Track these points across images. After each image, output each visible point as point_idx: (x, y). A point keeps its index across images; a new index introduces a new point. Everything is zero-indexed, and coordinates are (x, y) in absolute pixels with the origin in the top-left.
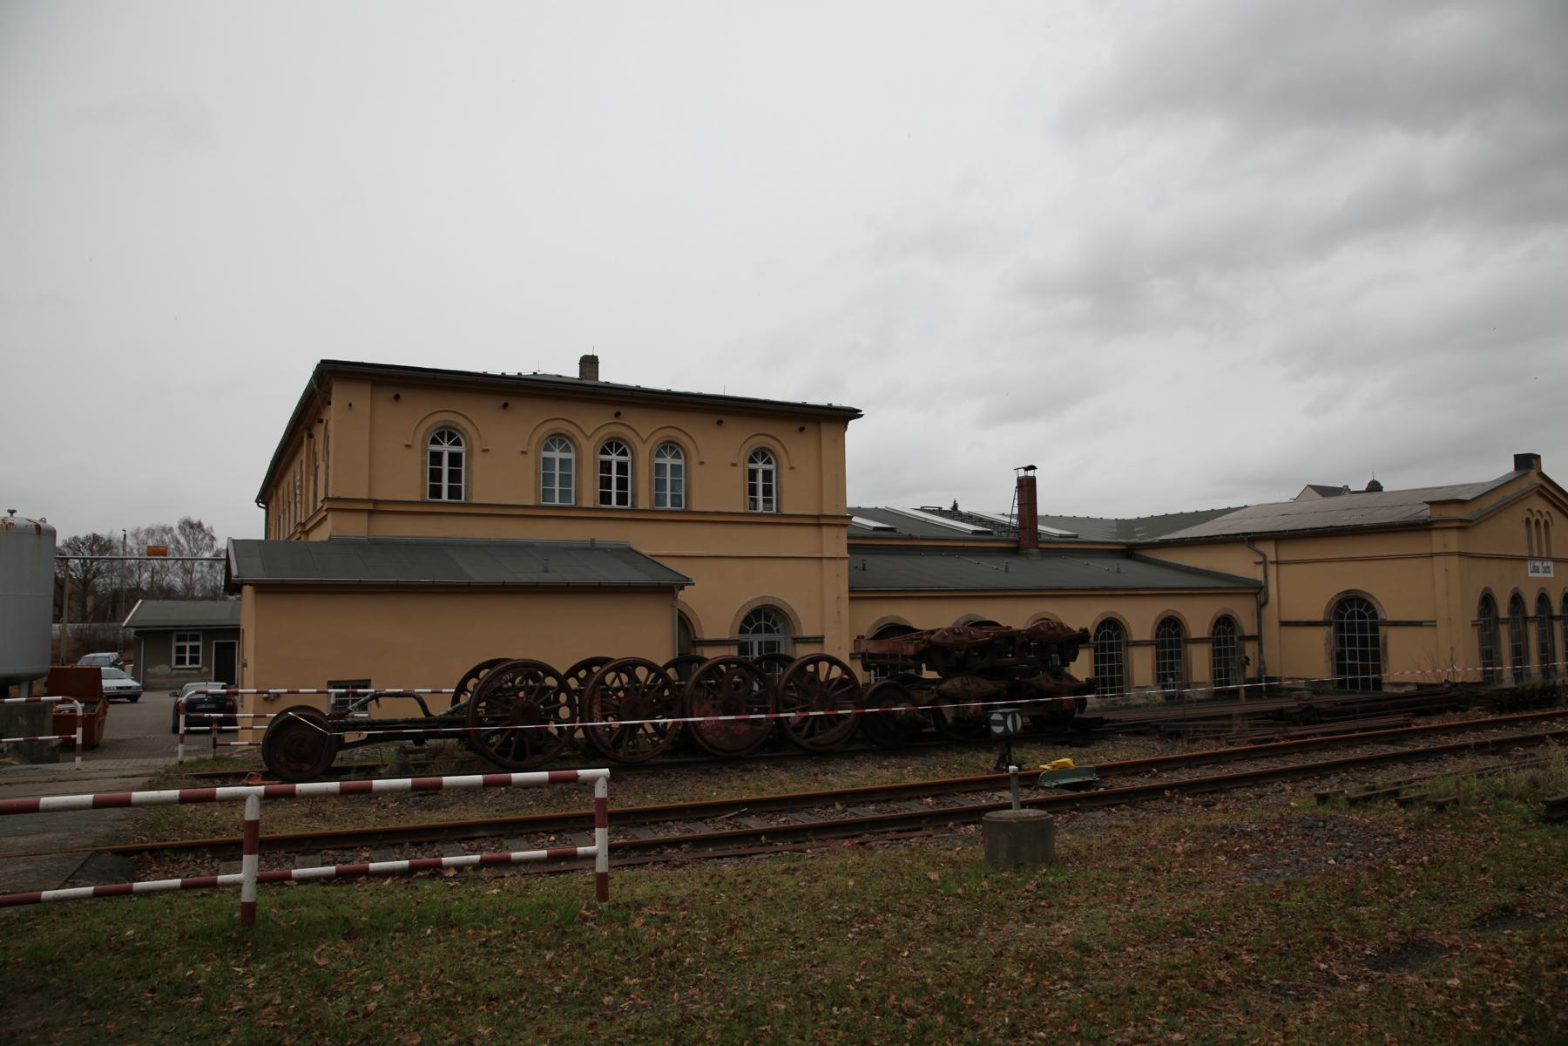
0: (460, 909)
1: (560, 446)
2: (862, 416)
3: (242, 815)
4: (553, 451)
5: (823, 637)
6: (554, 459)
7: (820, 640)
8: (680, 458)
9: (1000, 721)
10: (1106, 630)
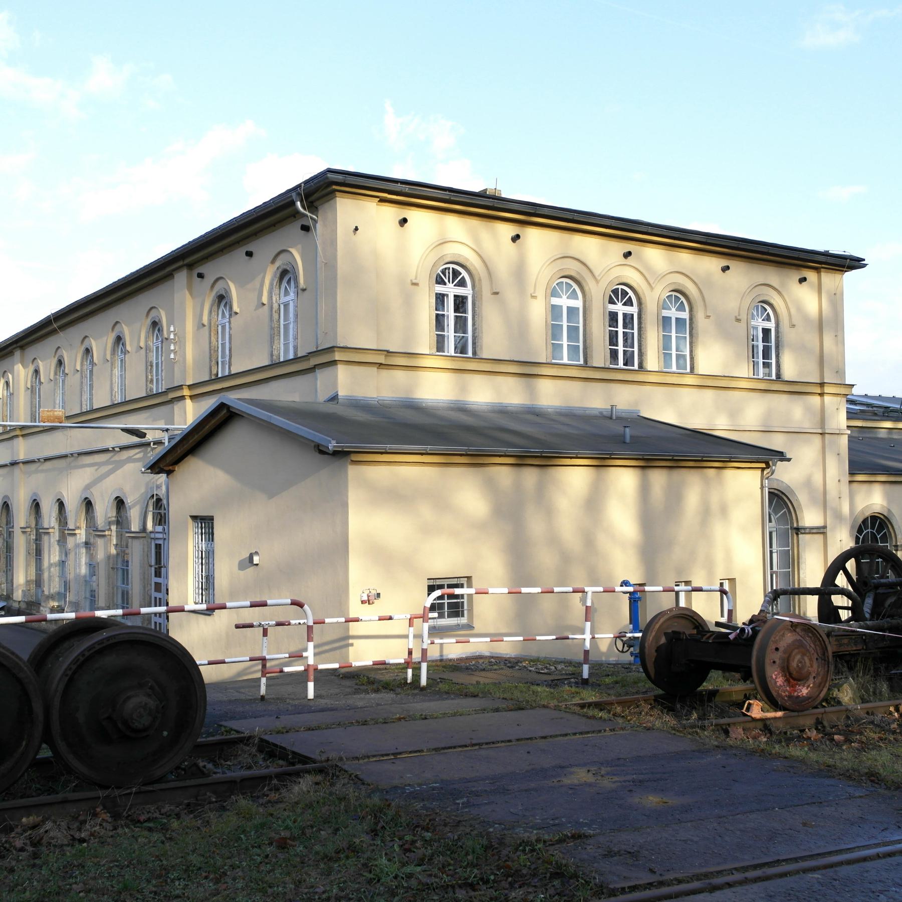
0: (208, 883)
1: (567, 292)
2: (865, 266)
3: (51, 757)
4: (561, 297)
5: (825, 527)
6: (671, 318)
7: (822, 530)
8: (577, 298)
9: (260, 692)
10: (869, 530)
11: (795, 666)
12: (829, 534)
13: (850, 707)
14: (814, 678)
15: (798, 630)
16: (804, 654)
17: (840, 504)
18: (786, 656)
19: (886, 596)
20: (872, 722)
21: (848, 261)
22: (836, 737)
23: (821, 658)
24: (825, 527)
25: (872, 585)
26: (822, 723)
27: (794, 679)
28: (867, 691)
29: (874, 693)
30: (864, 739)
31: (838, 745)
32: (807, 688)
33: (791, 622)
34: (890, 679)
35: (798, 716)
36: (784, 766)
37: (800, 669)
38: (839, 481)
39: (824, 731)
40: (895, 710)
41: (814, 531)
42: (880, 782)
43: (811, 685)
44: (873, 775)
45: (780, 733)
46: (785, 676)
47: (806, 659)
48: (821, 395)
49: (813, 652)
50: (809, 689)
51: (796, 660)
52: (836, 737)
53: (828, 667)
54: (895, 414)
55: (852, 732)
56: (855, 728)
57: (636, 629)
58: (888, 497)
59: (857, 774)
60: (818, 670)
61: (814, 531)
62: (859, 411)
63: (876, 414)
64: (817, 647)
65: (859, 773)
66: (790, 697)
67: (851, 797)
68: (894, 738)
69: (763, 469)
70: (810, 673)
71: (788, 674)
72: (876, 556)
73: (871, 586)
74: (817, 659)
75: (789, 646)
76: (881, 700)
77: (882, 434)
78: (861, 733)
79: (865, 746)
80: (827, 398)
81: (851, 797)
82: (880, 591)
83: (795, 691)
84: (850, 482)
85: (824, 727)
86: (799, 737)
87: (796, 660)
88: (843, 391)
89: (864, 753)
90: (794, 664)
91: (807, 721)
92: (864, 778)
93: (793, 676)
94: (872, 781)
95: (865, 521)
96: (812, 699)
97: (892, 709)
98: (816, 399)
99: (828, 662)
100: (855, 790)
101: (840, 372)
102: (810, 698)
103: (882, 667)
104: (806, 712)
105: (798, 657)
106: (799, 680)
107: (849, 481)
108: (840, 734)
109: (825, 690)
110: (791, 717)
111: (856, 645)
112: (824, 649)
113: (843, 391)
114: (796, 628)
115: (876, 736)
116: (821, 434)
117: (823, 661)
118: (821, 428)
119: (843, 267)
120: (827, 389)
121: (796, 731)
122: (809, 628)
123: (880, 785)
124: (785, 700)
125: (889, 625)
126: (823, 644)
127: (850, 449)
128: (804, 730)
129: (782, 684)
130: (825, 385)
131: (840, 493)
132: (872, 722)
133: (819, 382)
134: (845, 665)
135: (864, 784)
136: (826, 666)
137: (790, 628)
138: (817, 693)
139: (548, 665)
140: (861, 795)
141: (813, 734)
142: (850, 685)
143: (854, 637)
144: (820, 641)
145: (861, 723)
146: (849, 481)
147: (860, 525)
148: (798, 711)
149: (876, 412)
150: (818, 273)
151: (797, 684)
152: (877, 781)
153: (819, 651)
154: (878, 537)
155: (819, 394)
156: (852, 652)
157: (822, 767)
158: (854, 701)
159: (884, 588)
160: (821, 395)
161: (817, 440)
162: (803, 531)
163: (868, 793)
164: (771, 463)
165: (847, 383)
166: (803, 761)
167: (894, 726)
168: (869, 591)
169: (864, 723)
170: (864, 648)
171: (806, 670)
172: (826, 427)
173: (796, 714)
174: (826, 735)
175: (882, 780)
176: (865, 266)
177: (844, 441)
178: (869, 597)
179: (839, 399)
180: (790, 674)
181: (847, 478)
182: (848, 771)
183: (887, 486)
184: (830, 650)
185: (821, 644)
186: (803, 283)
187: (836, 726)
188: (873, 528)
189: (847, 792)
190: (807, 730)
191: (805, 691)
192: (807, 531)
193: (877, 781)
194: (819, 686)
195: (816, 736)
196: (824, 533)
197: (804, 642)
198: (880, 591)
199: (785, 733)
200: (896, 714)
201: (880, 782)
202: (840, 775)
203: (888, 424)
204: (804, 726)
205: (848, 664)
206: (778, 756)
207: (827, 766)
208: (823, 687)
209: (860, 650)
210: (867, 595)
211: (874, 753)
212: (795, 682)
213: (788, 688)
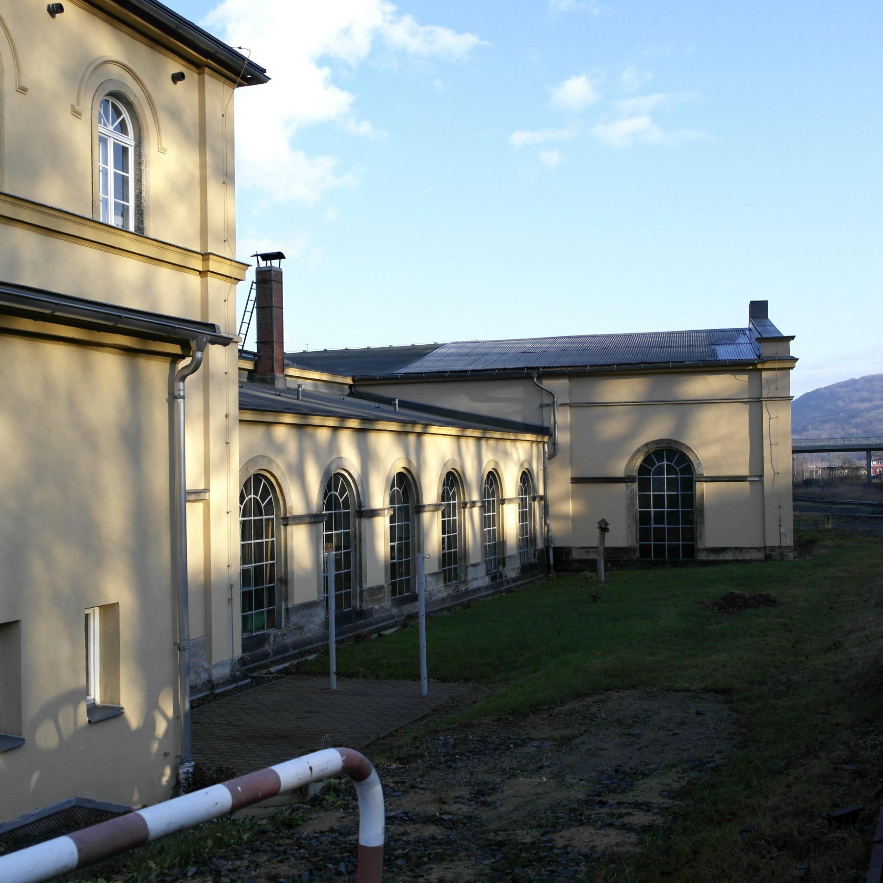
10: (252, 496)
48: (203, 273)
57: (763, 357)
69: (175, 358)
100: (877, 642)
139: (636, 719)
150: (199, 74)
154: (263, 505)
155: (200, 272)
162: (192, 497)
164: (193, 344)
186: (178, 83)
188: (256, 493)
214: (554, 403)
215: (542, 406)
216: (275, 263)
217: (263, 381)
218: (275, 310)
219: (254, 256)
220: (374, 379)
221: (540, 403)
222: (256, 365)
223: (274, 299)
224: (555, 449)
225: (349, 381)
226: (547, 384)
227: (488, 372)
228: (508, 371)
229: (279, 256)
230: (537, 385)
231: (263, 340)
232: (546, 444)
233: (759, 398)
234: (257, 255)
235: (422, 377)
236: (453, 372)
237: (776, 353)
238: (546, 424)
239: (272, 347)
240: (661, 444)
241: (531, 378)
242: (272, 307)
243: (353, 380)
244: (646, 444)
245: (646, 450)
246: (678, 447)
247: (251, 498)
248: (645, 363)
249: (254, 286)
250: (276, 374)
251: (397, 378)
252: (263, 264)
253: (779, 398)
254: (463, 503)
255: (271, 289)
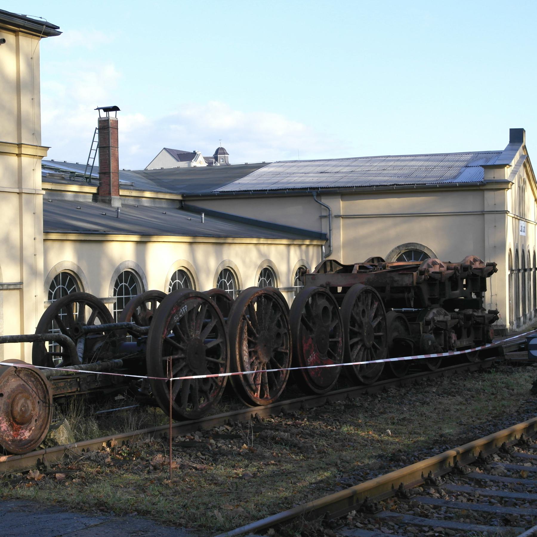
5: (21, 283)
7: (18, 287)
10: (61, 286)
11: (19, 410)
12: (25, 289)
13: (68, 447)
14: (36, 420)
15: (21, 375)
16: (27, 399)
17: (36, 261)
18: (11, 400)
19: (95, 341)
20: (89, 458)
21: (44, 27)
22: (58, 475)
23: (42, 401)
24: (21, 283)
25: (83, 331)
26: (43, 463)
27: (18, 423)
28: (79, 429)
29: (86, 433)
30: (83, 474)
31: (61, 482)
32: (30, 431)
33: (15, 367)
34: (98, 418)
35: (22, 459)
36: (19, 506)
37: (23, 413)
38: (35, 239)
39: (45, 471)
40: (107, 445)
41: (12, 287)
42: (109, 511)
43: (33, 428)
44: (101, 505)
45: (5, 476)
46: (10, 421)
47: (29, 402)
48: (19, 155)
49: (35, 395)
50: (31, 432)
51: (20, 405)
52: (58, 475)
53: (49, 409)
54: (80, 179)
55: (71, 469)
56: (74, 465)
58: (79, 256)
59: (87, 505)
60: (39, 413)
61: (12, 287)
62: (48, 175)
63: (63, 179)
64: (39, 390)
65: (89, 504)
66: (13, 441)
67: (87, 527)
68: (110, 471)
70: (32, 416)
71: (11, 419)
72: (85, 303)
73: (82, 332)
74: (39, 402)
75: (13, 391)
76: (91, 438)
77: (69, 197)
78: (80, 470)
79: (86, 481)
80: (24, 159)
81: (87, 527)
82: (89, 336)
83: (18, 435)
84: (45, 240)
85: (45, 467)
86: (23, 478)
87: (20, 405)
88: (40, 153)
89: (86, 487)
90: (18, 409)
91: (28, 462)
92: (94, 509)
93: (17, 420)
94: (102, 510)
95: (56, 278)
96: (34, 441)
97: (104, 445)
98: (14, 160)
99: (49, 404)
101: (36, 134)
102: (32, 441)
103: (92, 406)
104: (28, 455)
105: (22, 401)
106: (22, 424)
107: (44, 240)
108: (61, 472)
109: (46, 431)
110: (13, 460)
111: (71, 388)
112: (46, 392)
113: (40, 153)
114: (20, 373)
115: (94, 470)
116: (18, 193)
117: (44, 404)
118: (18, 188)
119: (40, 32)
120: (24, 150)
121: (19, 474)
122: (31, 373)
123: (110, 513)
124: (9, 444)
125: (100, 367)
126: (44, 387)
127: (44, 211)
128: (28, 471)
129: (6, 429)
130: (23, 146)
131: (35, 249)
132: (89, 458)
133: (16, 143)
134: (59, 408)
135: (95, 514)
136: (47, 408)
137: (14, 373)
138: (39, 435)
140: (96, 523)
141: (36, 475)
142: (66, 426)
143: (69, 380)
144: (41, 384)
145: (78, 460)
146: (44, 240)
147: (53, 281)
148: (21, 454)
149: (63, 176)
151: (20, 428)
152: (106, 510)
153: (40, 395)
156: (67, 395)
157: (54, 504)
158: (69, 441)
159: (92, 333)
160: (19, 155)
161: (15, 199)
163: (102, 521)
165: (42, 145)
166: (35, 500)
167: (109, 460)
168: (80, 337)
169: (81, 460)
170: (79, 390)
171: (29, 413)
172: (23, 187)
173: (19, 457)
174: (47, 475)
175: (112, 508)
176: (59, 33)
177: (39, 200)
178: (80, 342)
179: (35, 160)
180: (14, 418)
181: (41, 237)
182: (78, 504)
183: (78, 245)
184: (51, 392)
185: (43, 387)
187: (56, 465)
188: (64, 284)
189: (82, 523)
190: (31, 471)
191: (27, 435)
192: (5, 287)
193: (106, 510)
194: (41, 428)
195: (39, 476)
196: (21, 290)
197: (27, 386)
198: (89, 336)
199: (10, 476)
200: (108, 449)
201: (109, 511)
202: (72, 508)
203: (74, 188)
204: (26, 468)
205: (61, 407)
206: (11, 498)
207: (57, 502)
208: (45, 429)
209: (74, 392)
210: (79, 340)
211: (95, 486)
212: (19, 426)
213: (11, 433)
214: (329, 215)
215: (322, 217)
216: (112, 114)
217: (104, 201)
218: (112, 149)
219: (97, 109)
220: (197, 196)
221: (320, 215)
222: (98, 190)
223: (111, 141)
224: (330, 250)
225: (179, 198)
226: (325, 201)
227: (281, 191)
228: (296, 191)
229: (116, 109)
230: (317, 202)
231: (103, 171)
232: (324, 247)
233: (482, 212)
234: (99, 109)
235: (233, 195)
236: (256, 191)
237: (494, 178)
238: (324, 231)
239: (110, 177)
240: (409, 247)
241: (312, 196)
242: (109, 147)
243: (183, 196)
244: (398, 247)
245: (398, 251)
246: (422, 249)
247: (60, 288)
248: (397, 185)
249: (97, 131)
250: (112, 196)
251: (214, 195)
252: (104, 114)
253: (496, 211)
254: (238, 291)
255: (108, 134)
